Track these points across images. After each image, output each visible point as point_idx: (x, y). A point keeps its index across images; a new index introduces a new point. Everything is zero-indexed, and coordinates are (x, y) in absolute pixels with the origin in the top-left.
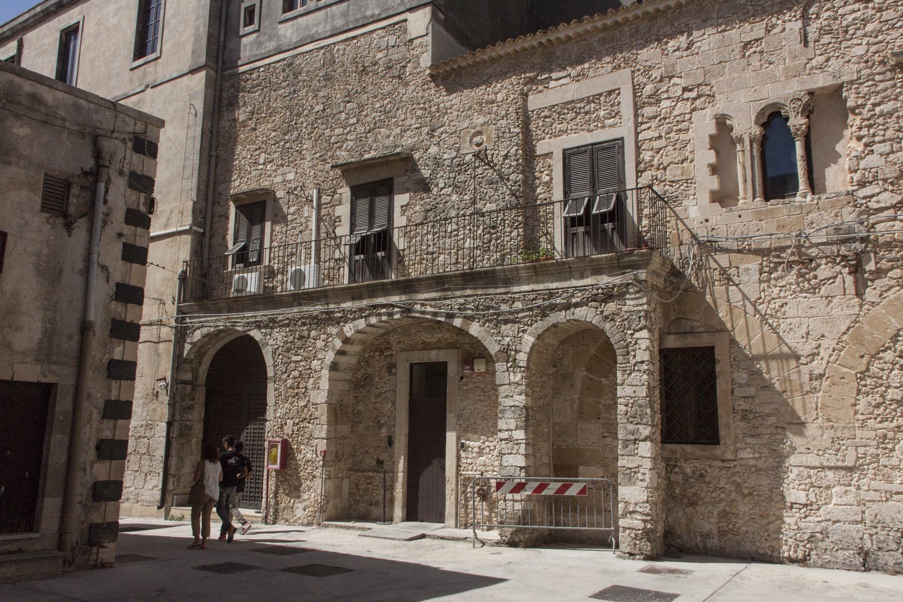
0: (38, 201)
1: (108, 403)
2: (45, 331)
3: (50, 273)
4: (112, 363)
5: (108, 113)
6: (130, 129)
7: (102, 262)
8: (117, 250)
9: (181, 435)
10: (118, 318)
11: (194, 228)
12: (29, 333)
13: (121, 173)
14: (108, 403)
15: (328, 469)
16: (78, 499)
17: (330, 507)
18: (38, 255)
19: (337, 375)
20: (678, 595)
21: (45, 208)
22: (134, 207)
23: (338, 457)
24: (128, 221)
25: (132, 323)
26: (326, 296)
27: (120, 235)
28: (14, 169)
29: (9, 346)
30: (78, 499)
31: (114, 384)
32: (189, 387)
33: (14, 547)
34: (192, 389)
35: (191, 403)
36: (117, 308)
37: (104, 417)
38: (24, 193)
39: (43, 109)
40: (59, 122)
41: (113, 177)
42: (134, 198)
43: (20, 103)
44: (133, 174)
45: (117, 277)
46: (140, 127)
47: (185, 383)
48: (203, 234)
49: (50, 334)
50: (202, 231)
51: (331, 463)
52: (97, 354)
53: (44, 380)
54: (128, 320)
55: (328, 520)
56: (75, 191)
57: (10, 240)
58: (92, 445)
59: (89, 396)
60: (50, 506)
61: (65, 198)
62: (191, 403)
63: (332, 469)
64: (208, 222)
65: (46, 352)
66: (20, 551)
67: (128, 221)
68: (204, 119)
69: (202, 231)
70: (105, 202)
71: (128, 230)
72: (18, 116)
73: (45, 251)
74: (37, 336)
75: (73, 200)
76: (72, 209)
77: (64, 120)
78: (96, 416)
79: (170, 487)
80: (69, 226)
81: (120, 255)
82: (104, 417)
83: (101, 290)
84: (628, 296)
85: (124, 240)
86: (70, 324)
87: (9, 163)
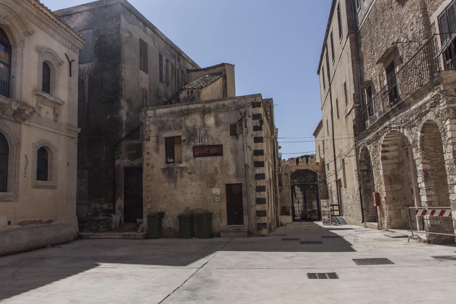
0: (229, 133)
1: (257, 187)
2: (236, 169)
3: (235, 152)
4: (257, 175)
5: (243, 100)
6: (250, 101)
7: (248, 145)
8: (252, 140)
9: (365, 193)
10: (256, 161)
11: (355, 105)
12: (232, 171)
13: (249, 116)
14: (257, 187)
15: (389, 205)
16: (253, 216)
17: (393, 222)
18: (231, 148)
19: (387, 162)
20: (354, 260)
21: (231, 135)
22: (256, 125)
23: (394, 199)
24: (254, 130)
25: (261, 162)
26: (375, 127)
27: (252, 135)
28: (222, 127)
29: (228, 175)
30: (253, 216)
31: (258, 181)
32: (366, 172)
33: (238, 228)
34: (368, 173)
35: (368, 179)
36: (255, 158)
37: (256, 191)
38: (225, 132)
39: (226, 107)
40: (230, 109)
41: (247, 119)
42: (255, 122)
43: (219, 109)
44: (253, 115)
45: (253, 148)
46: (253, 99)
47: (364, 171)
48: (360, 106)
49: (237, 169)
50: (359, 105)
51: (390, 203)
52: (251, 172)
53: (238, 183)
54: (259, 161)
55: (393, 228)
56: (238, 127)
57: (223, 146)
58: (254, 200)
59: (250, 186)
60: (245, 217)
61: (236, 130)
62: (368, 179)
63: (391, 205)
64: (361, 100)
65: (237, 175)
66: (239, 229)
67: (254, 130)
68: (352, 57)
69: (359, 105)
70: (246, 127)
71: (255, 133)
72: (220, 112)
73: (233, 147)
74: (234, 171)
75: (238, 130)
76: (238, 133)
77: (231, 108)
78: (254, 191)
79: (365, 214)
80: (237, 138)
81: (253, 141)
82: (256, 191)
83: (249, 153)
84: (440, 101)
85: (254, 136)
86: (242, 167)
87: (220, 126)
